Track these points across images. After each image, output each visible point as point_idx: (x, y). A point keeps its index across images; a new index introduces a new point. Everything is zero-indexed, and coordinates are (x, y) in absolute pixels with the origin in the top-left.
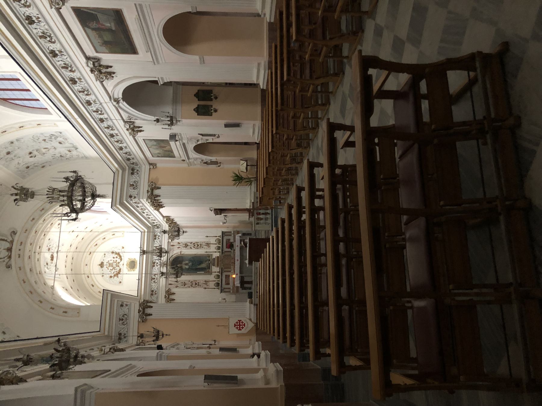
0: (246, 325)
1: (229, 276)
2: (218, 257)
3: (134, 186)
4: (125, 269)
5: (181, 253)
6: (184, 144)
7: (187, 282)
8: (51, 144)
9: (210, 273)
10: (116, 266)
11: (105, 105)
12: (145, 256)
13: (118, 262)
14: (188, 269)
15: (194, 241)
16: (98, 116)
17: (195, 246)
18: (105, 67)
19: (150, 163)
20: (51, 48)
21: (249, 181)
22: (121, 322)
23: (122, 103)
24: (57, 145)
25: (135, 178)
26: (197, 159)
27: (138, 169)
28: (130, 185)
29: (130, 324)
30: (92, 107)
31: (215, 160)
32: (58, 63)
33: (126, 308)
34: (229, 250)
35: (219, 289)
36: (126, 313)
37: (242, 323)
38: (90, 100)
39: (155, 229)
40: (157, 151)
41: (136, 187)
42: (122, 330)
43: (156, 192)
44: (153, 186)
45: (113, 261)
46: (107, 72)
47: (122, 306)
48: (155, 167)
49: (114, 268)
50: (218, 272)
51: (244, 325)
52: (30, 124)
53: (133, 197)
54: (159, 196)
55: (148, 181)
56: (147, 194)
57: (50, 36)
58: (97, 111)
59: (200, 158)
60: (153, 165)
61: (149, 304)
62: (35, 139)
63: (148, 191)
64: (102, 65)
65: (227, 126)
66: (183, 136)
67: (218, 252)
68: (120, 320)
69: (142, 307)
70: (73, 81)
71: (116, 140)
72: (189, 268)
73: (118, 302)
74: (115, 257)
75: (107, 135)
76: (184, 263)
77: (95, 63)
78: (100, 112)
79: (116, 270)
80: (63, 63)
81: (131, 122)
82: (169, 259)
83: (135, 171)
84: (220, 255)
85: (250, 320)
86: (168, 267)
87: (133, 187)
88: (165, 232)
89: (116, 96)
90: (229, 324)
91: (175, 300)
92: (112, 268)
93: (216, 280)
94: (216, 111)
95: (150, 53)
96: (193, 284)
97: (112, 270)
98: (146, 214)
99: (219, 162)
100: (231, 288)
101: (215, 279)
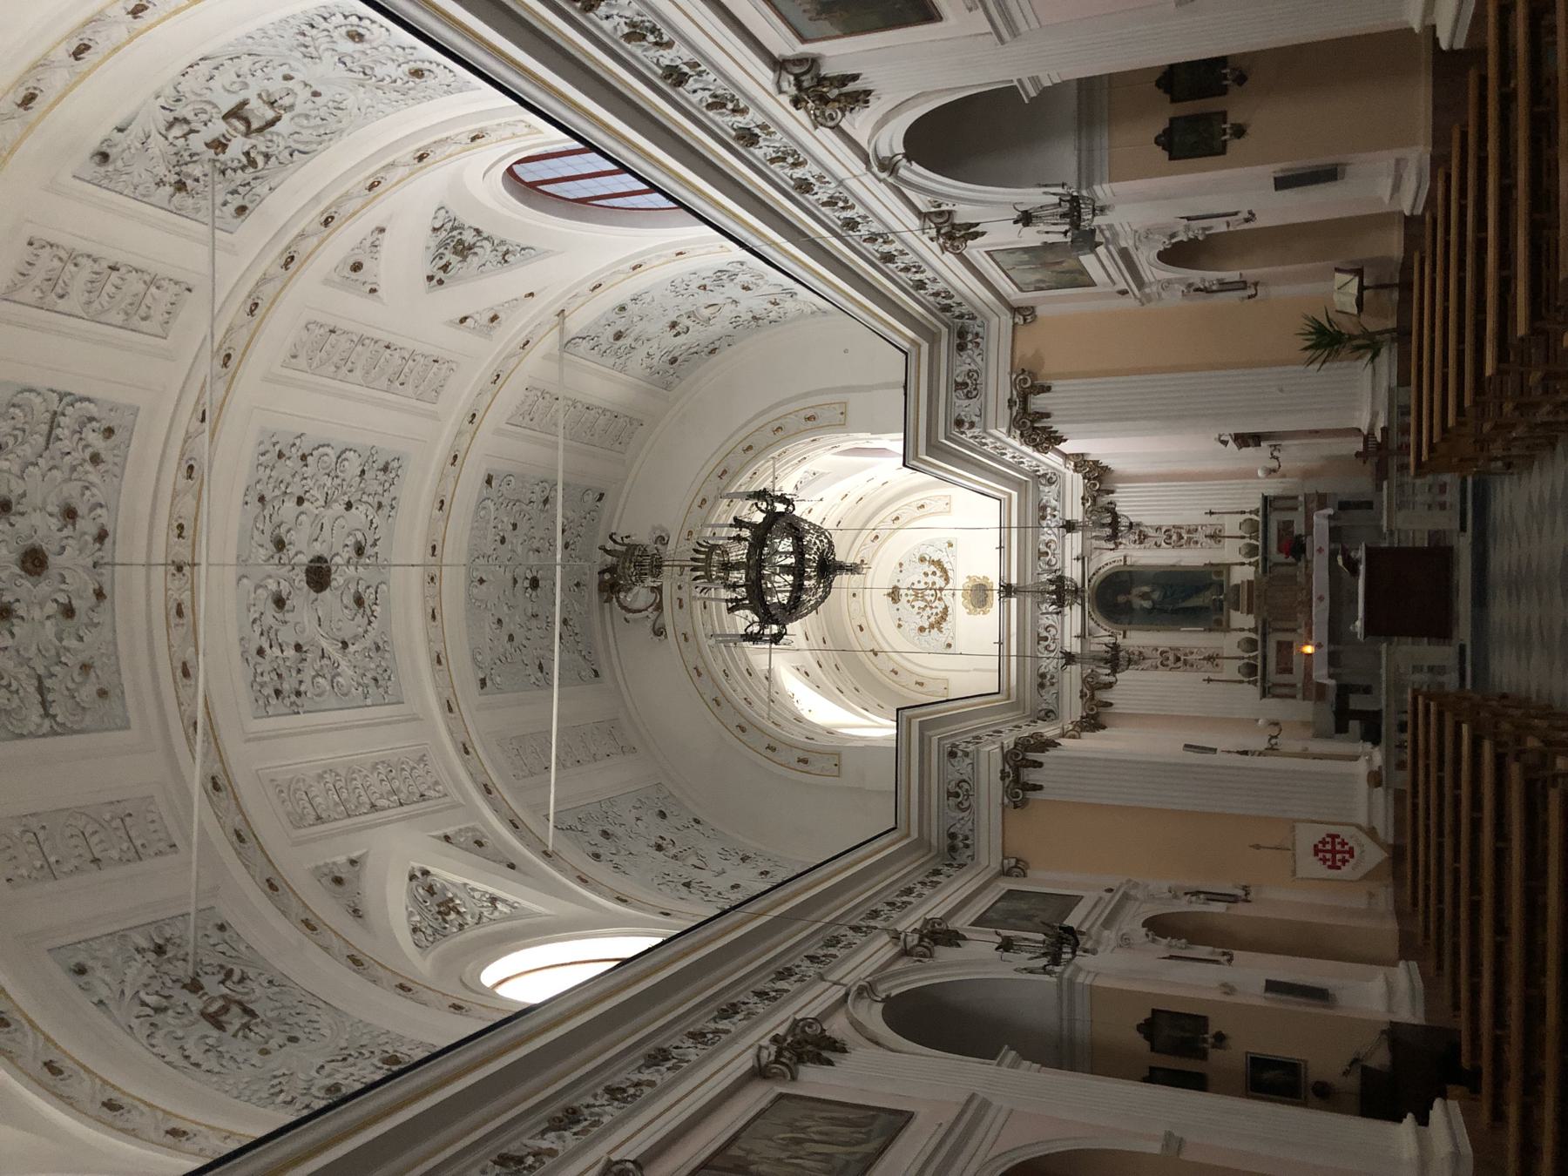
0: (1357, 852)
1: (1290, 645)
2: (1248, 581)
3: (967, 387)
4: (959, 607)
5: (1125, 561)
6: (1124, 254)
7: (1147, 652)
8: (722, 293)
9: (1222, 626)
10: (933, 599)
11: (853, 184)
12: (1014, 601)
13: (937, 586)
14: (1150, 611)
15: (1168, 521)
16: (837, 214)
17: (1170, 537)
18: (836, 84)
19: (1015, 306)
20: (665, 62)
21: (1370, 345)
22: (953, 801)
23: (905, 167)
24: (738, 293)
25: (968, 360)
26: (1169, 282)
27: (977, 329)
28: (957, 384)
29: (978, 810)
30: (816, 193)
31: (1237, 278)
32: (695, 98)
33: (966, 763)
34: (1291, 559)
35: (1254, 683)
36: (965, 777)
37: (1343, 844)
38: (808, 176)
39: (1041, 487)
40: (1033, 277)
41: (975, 389)
42: (958, 826)
43: (1038, 402)
44: (1025, 383)
45: (926, 583)
46: (847, 95)
47: (952, 754)
48: (1029, 319)
49: (929, 605)
50: (1250, 630)
51: (1351, 852)
52: (659, 256)
53: (967, 425)
54: (1048, 415)
55: (1009, 370)
56: (1009, 411)
57: (653, 30)
58: (831, 203)
59: (1180, 279)
60: (1023, 313)
61: (1032, 756)
62: (676, 287)
63: (1011, 403)
64: (825, 78)
65: (1282, 183)
66: (1118, 228)
67: (1250, 564)
68: (950, 794)
69: (1012, 763)
70: (748, 137)
71: (902, 266)
72: (1153, 608)
73: (942, 743)
74: (930, 573)
75: (871, 257)
76: (1135, 591)
77: (803, 78)
78: (841, 204)
79: (934, 611)
80: (707, 94)
81: (941, 214)
82: (1089, 581)
83: (970, 337)
84: (1256, 577)
85: (1371, 833)
86: (1087, 604)
87: (965, 391)
88: (1070, 526)
89: (884, 152)
90: (1294, 844)
91: (1111, 704)
92: (922, 604)
93: (1246, 655)
94: (1239, 131)
95: (981, 9)
96: (1168, 659)
97: (924, 609)
98: (1009, 455)
99: (1250, 280)
100: (1299, 685)
101: (1239, 653)
